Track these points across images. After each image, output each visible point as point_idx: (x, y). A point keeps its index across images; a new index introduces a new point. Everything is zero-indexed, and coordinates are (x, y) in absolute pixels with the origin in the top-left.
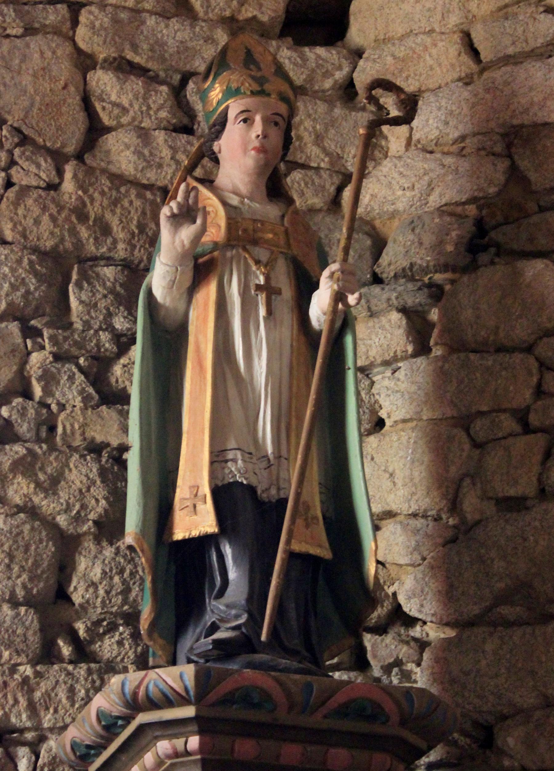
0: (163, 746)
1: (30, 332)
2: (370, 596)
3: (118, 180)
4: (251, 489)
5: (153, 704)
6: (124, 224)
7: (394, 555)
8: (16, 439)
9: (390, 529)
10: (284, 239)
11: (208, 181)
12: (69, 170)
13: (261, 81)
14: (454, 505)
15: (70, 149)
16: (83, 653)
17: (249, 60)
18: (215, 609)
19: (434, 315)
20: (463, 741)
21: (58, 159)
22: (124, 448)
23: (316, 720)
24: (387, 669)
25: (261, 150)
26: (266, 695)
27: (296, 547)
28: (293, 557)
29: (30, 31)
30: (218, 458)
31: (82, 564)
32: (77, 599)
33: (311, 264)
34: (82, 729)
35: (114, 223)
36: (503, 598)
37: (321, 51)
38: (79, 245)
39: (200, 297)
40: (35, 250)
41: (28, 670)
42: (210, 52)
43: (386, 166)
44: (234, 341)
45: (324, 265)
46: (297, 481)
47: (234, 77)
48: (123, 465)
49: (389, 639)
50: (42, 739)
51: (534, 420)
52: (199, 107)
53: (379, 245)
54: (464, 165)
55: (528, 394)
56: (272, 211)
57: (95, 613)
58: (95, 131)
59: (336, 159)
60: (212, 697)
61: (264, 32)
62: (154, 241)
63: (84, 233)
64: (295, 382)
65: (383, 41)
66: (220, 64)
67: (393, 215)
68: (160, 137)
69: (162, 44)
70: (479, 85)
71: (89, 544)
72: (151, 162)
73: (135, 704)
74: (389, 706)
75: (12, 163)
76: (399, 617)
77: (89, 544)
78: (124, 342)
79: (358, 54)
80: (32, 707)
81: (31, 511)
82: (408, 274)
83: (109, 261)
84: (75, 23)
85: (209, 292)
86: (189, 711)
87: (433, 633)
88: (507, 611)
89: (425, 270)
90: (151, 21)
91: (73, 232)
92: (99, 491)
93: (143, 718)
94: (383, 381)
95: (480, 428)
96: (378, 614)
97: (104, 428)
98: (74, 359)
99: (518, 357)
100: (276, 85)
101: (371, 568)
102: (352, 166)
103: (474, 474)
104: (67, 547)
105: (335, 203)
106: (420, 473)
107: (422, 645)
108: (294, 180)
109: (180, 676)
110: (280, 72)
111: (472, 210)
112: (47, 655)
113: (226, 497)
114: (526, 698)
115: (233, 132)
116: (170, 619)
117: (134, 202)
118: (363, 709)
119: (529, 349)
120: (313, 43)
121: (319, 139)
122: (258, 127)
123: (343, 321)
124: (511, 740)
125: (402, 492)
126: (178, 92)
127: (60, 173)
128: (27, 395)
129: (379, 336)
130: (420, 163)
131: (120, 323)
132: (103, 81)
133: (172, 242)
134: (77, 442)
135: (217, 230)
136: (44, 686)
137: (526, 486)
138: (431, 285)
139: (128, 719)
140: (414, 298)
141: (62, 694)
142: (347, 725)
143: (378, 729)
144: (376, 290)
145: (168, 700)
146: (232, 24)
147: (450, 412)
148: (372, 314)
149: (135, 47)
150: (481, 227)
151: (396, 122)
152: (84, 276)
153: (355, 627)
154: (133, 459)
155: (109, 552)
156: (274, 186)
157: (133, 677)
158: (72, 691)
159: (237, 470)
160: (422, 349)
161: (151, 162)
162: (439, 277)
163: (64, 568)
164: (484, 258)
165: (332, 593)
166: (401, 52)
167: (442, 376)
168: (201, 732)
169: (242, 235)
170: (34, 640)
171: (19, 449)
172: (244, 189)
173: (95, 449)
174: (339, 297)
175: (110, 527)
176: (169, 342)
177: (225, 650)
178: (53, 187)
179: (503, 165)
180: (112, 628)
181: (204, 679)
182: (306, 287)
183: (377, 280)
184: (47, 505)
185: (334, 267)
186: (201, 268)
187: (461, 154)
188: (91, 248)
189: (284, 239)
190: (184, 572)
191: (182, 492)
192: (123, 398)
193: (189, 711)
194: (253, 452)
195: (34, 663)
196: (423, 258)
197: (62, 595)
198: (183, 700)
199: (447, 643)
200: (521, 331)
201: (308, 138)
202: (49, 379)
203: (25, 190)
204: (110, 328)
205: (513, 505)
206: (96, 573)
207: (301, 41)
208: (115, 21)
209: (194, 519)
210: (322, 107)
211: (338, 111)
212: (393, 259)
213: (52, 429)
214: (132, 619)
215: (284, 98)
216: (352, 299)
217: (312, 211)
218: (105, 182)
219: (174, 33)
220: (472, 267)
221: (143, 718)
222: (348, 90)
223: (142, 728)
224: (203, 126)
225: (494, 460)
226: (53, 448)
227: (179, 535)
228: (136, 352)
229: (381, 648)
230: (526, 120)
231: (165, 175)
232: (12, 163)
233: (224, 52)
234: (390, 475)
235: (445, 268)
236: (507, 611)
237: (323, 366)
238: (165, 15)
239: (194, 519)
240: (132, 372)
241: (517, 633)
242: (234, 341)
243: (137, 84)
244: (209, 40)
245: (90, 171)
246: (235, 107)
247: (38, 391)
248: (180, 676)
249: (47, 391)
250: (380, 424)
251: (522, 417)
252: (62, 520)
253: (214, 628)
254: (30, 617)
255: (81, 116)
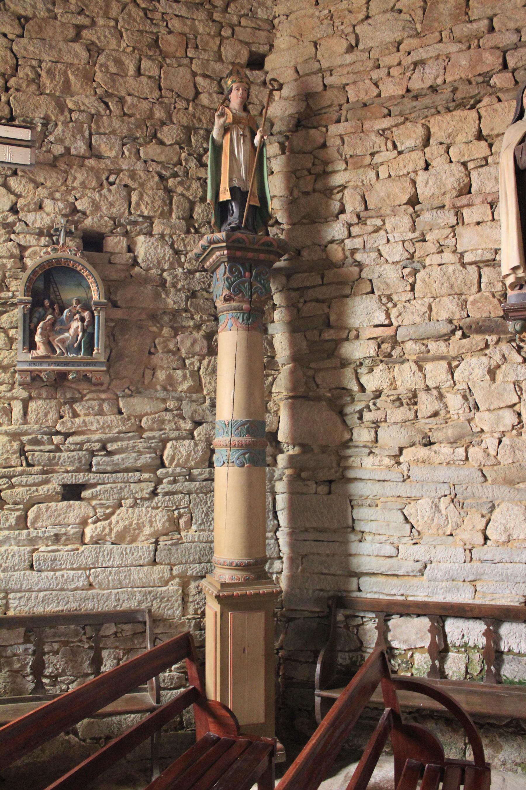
0: (218, 253)
1: (181, 148)
2: (270, 216)
3: (204, 107)
4: (239, 188)
5: (215, 242)
6: (206, 119)
7: (276, 206)
8: (178, 176)
9: (275, 200)
10: (248, 122)
11: (228, 107)
12: (191, 104)
13: (241, 79)
14: (291, 194)
15: (191, 98)
16: (197, 231)
17: (238, 73)
18: (230, 219)
19: (287, 144)
20: (293, 254)
21: (188, 101)
22: (206, 179)
23: (256, 247)
24: (274, 236)
25: (242, 98)
26: (244, 240)
27: (251, 203)
28: (250, 206)
29: (180, 65)
30: (231, 180)
31: (196, 209)
32: (195, 218)
33: (254, 129)
34: (197, 250)
35: (203, 118)
36: (304, 218)
37: (257, 72)
38: (194, 124)
39: (226, 137)
40: (182, 126)
41: (183, 236)
42: (228, 72)
43: (274, 104)
44: (235, 150)
45: (258, 128)
46: (251, 187)
47: (234, 78)
48: (206, 183)
49: (274, 228)
50: (187, 253)
51: (312, 172)
52: (225, 87)
53: (272, 125)
54: (295, 104)
55: (311, 165)
56: (244, 114)
57: (200, 221)
58: (197, 93)
59: (261, 102)
60: (231, 240)
61: (242, 66)
62: (213, 124)
63: (195, 121)
64: (250, 255)
65: (273, 69)
66: (230, 74)
67: (276, 117)
68: (215, 95)
69: (215, 70)
70: (299, 82)
71: (198, 204)
72: (212, 102)
73: (211, 243)
74: (275, 244)
75: (176, 102)
76: (277, 223)
77: (198, 204)
78: (206, 151)
79: (267, 73)
80: (184, 245)
81: (183, 195)
82: (280, 133)
83: (202, 129)
84: (192, 63)
85: (228, 136)
86: (224, 244)
87: (286, 227)
88: (305, 221)
89: (284, 132)
90: (212, 63)
91: (192, 121)
92: (200, 190)
93: (212, 246)
94: (273, 161)
95: (298, 174)
96: (271, 222)
97: (201, 173)
98: (193, 155)
99: (308, 155)
100: (245, 80)
101: (270, 209)
102: (265, 104)
103: (297, 186)
104: (192, 204)
105: (261, 114)
106: (283, 186)
107: (283, 230)
108: (250, 107)
109: (221, 235)
110: (247, 77)
111: (297, 116)
112: (188, 232)
113: (233, 190)
114: (309, 243)
115: (234, 92)
116: (219, 222)
117: (208, 113)
118: (269, 244)
119: (311, 153)
120: (255, 70)
121: (257, 96)
122: (241, 91)
123: (263, 145)
124: (305, 253)
125: (278, 190)
126: (219, 83)
127: (188, 105)
128: (181, 165)
129: (272, 149)
130: (283, 103)
131: (205, 146)
132: (199, 80)
133: (218, 122)
134: (194, 177)
135: (230, 120)
136: (187, 240)
137: (310, 189)
138: (286, 136)
139: (209, 247)
140: (282, 139)
141: (192, 242)
142: (264, 248)
143: (271, 249)
144: (271, 137)
145: (219, 242)
146: (233, 64)
147: (290, 169)
148: (271, 143)
149: (208, 70)
150: (299, 121)
151: (277, 90)
152: (195, 133)
153: (266, 225)
154: (209, 181)
155: (203, 206)
156: (245, 108)
157: (210, 236)
158: (194, 241)
159: (236, 183)
160: (283, 153)
161: (212, 102)
162: (288, 134)
163: (192, 210)
164: (300, 128)
165: (260, 215)
166: (278, 72)
167: (289, 159)
168: (228, 250)
169: (236, 121)
170: (185, 228)
171: (179, 179)
172: (237, 108)
173: (199, 179)
174: (262, 137)
175: (203, 199)
176: (218, 150)
177: (233, 229)
178: (186, 109)
179: (305, 103)
180: (204, 225)
181: (227, 236)
182: (253, 135)
183: (272, 134)
184: (187, 193)
185: (261, 129)
186: (226, 130)
187: (294, 100)
188: (197, 125)
189: (248, 122)
190: (222, 210)
191: (222, 189)
192: (206, 165)
193: (224, 244)
194: (240, 178)
195: (185, 234)
196: (284, 128)
197: (191, 217)
198: (223, 241)
199: (289, 230)
200: (309, 148)
201: (254, 96)
202: (187, 160)
203: (179, 110)
204: (202, 147)
205: (306, 194)
206: (200, 211)
207: (252, 69)
208: (202, 63)
209: (225, 196)
210: (257, 87)
211: (262, 89)
212: (276, 129)
213: (188, 174)
214: (209, 223)
215: (247, 83)
216: (265, 138)
217: (255, 116)
218: (200, 108)
219: (218, 66)
220: (297, 131)
221: (212, 246)
222: (264, 83)
223: (212, 249)
224: (226, 92)
225: (302, 182)
226: (188, 179)
227: (221, 200)
228: (209, 153)
229: (273, 231)
230: (311, 91)
231: (216, 106)
232: (176, 102)
233: (231, 71)
234: (275, 187)
235: (289, 131)
236: (305, 221)
237: (258, 156)
238: (216, 62)
239: (225, 196)
240: (208, 159)
241: (307, 226)
242: (235, 150)
243: (208, 81)
244: (227, 68)
245: (196, 105)
246: (234, 86)
247: (184, 163)
248: (221, 235)
249: (186, 164)
250: (272, 173)
251: (309, 171)
252: (191, 197)
253: (230, 224)
254: (183, 222)
255: (194, 89)
